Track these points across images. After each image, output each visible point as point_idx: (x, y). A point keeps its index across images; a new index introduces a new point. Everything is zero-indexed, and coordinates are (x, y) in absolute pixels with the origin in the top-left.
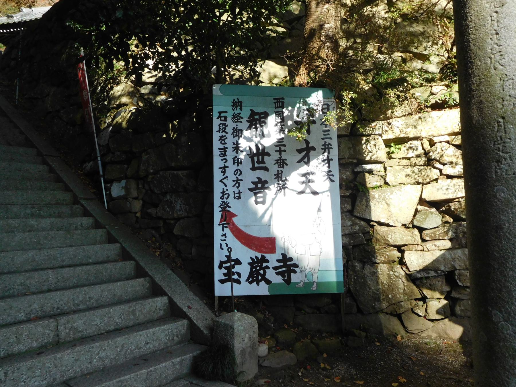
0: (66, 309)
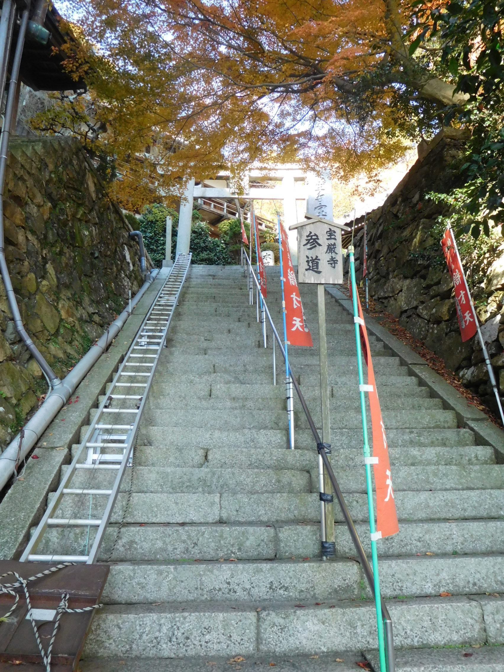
0: (486, 588)
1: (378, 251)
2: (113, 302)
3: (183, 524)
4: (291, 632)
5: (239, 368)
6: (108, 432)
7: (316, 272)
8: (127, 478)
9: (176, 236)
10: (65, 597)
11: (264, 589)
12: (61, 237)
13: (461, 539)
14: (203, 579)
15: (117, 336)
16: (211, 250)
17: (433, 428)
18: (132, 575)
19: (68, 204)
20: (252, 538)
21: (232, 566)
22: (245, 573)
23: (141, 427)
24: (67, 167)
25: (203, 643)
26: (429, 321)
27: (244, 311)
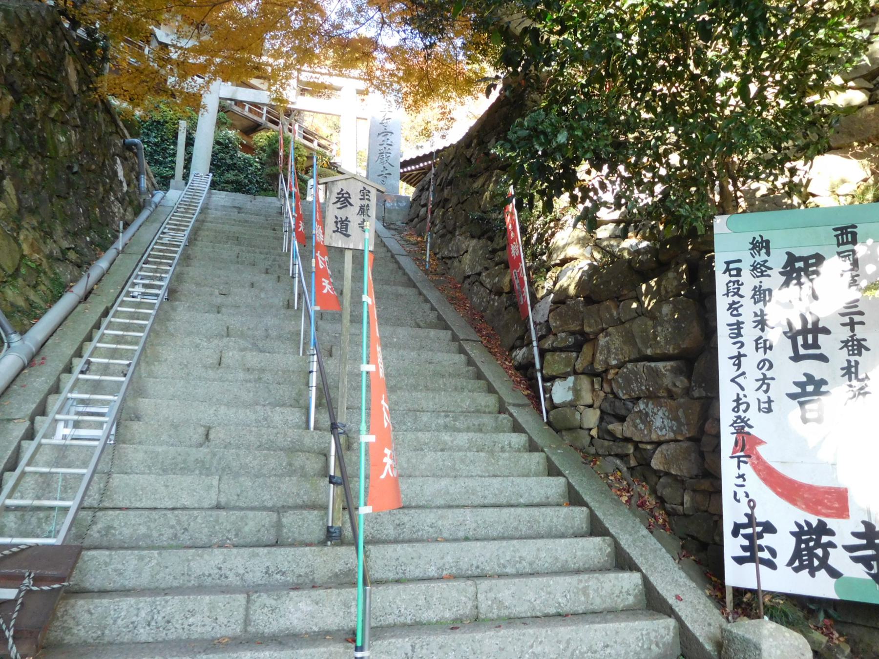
1: (447, 200)
2: (95, 233)
3: (173, 509)
4: (282, 613)
5: (260, 333)
6: (83, 402)
7: (345, 235)
8: (107, 458)
9: (193, 145)
10: (29, 576)
11: (259, 574)
12: (26, 143)
13: (474, 525)
14: (192, 564)
15: (100, 280)
16: (241, 170)
17: (473, 412)
18: (108, 560)
19: (37, 98)
20: (251, 524)
21: (225, 550)
22: (239, 558)
23: (128, 399)
24: (38, 47)
25: (186, 626)
26: (491, 291)
27: (274, 260)
